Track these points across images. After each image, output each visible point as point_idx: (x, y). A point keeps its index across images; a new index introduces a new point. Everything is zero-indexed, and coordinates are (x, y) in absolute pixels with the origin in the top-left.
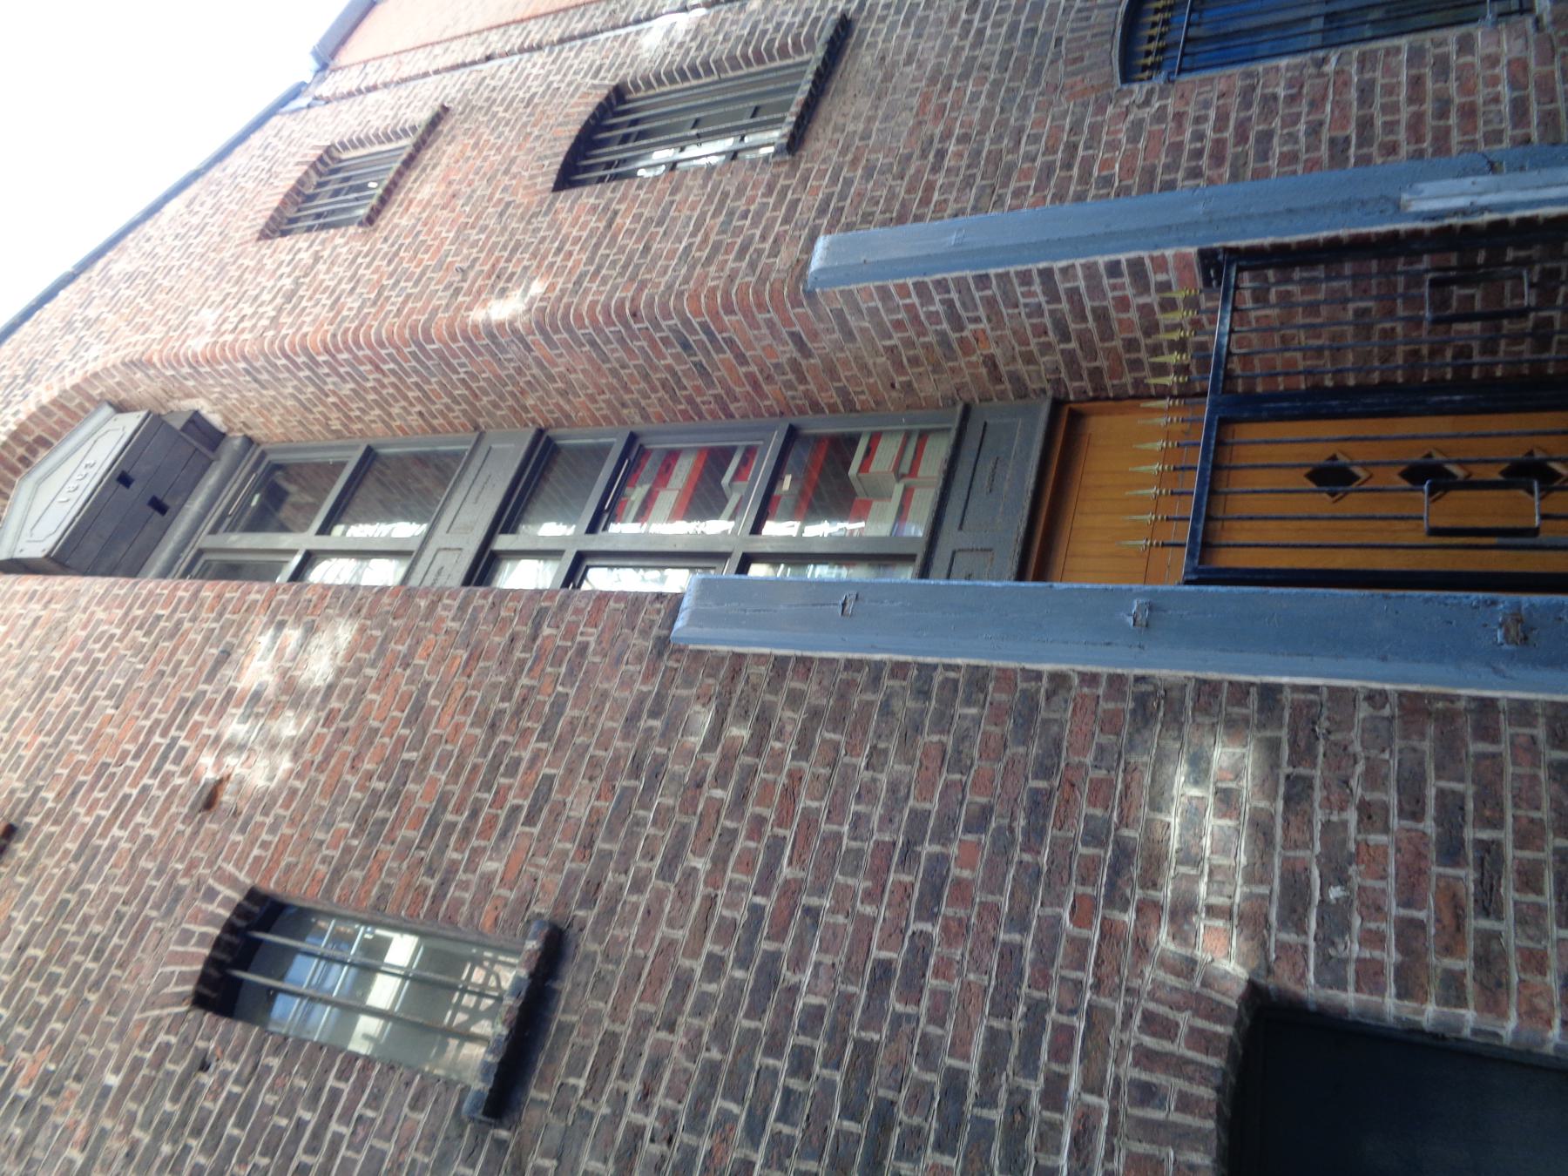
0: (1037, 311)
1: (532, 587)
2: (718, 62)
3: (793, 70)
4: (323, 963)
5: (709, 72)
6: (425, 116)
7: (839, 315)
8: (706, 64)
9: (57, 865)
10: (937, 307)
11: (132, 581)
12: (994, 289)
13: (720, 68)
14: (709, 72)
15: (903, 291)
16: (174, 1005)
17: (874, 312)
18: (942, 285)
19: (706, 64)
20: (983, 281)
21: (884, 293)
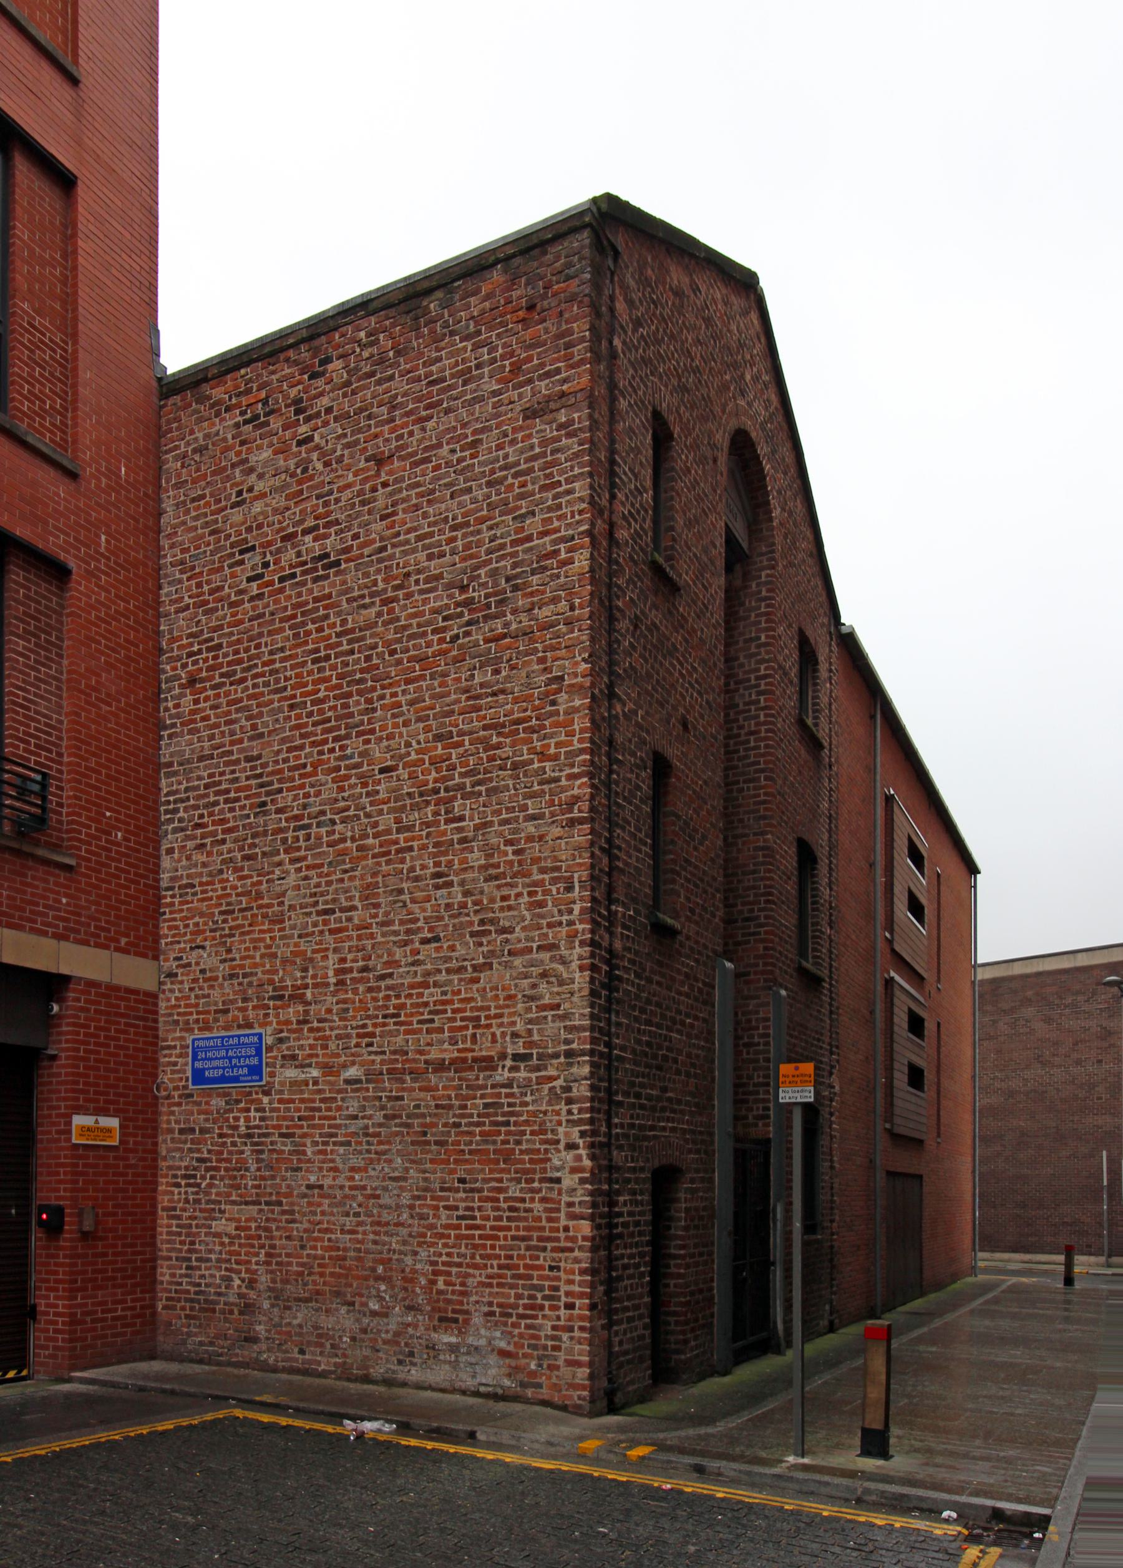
0: (750, 1077)
1: (160, 327)
2: (817, 916)
3: (879, 1015)
4: (1062, 1268)
5: (813, 910)
6: (822, 734)
7: (758, 997)
8: (817, 909)
9: (209, 1152)
10: (756, 1040)
11: (79, 183)
12: (762, 1063)
13: (814, 916)
14: (813, 910)
15: (767, 1028)
16: (726, 1415)
17: (757, 1012)
18: (767, 1044)
19: (817, 909)
20: (768, 1060)
21: (767, 1020)
